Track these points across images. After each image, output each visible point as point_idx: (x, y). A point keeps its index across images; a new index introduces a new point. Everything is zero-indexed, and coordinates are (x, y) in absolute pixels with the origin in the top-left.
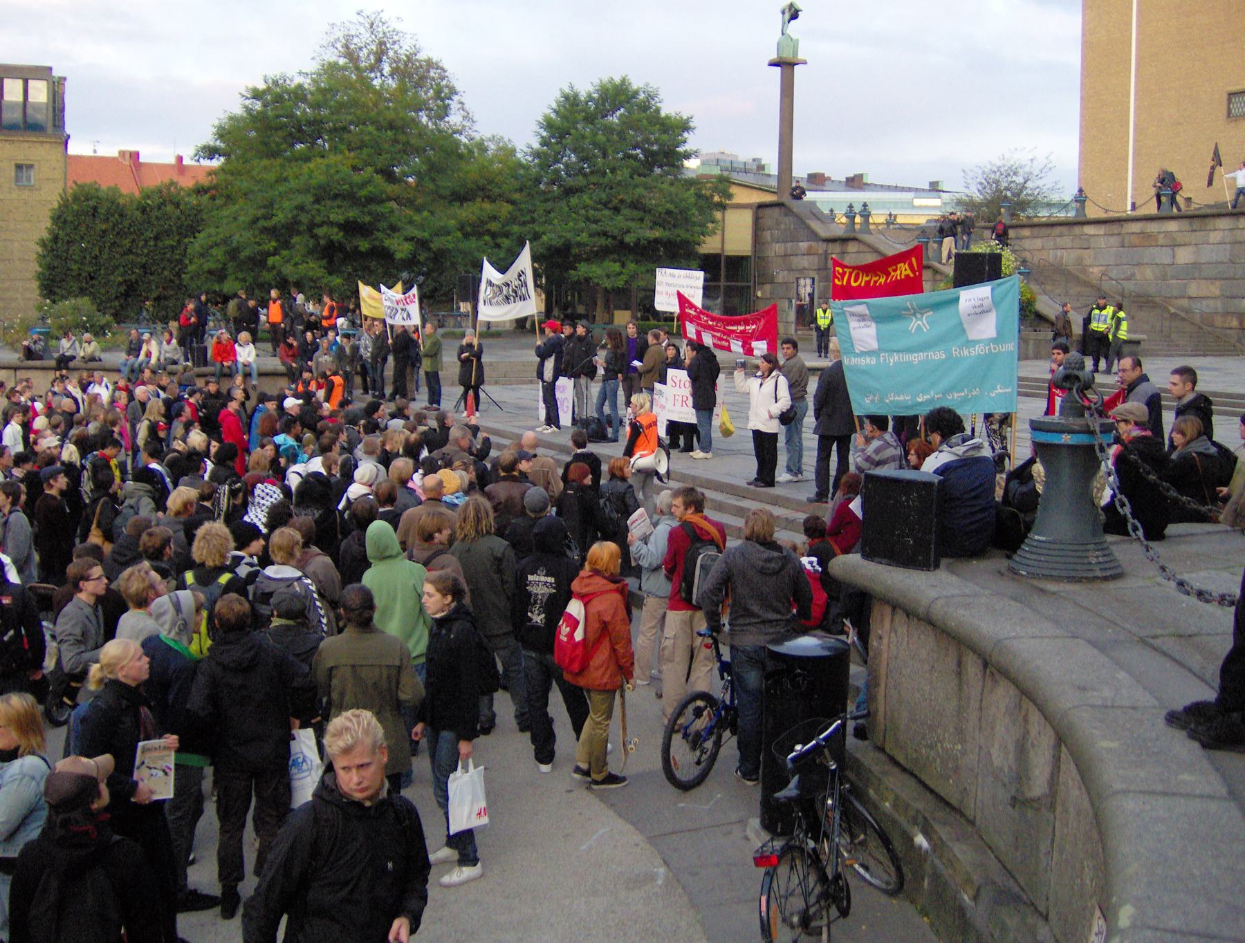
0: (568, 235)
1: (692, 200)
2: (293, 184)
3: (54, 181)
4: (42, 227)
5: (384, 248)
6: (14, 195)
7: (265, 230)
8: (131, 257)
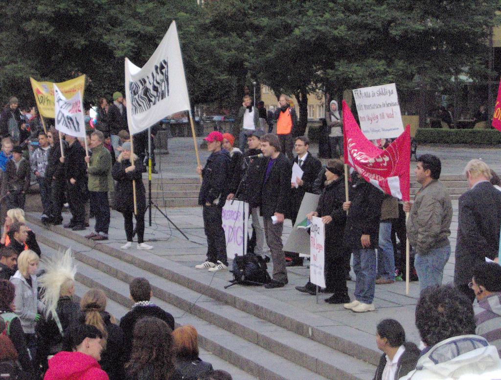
0: (323, 28)
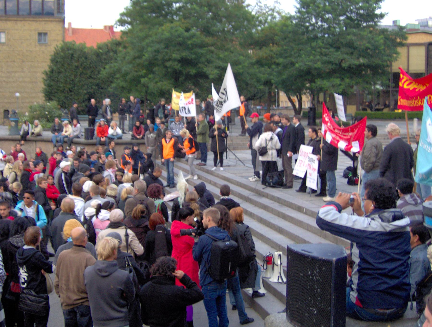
0: (310, 64)
1: (382, 41)
2: (154, 38)
3: (58, 41)
4: (45, 65)
5: (205, 73)
6: (37, 49)
7: (138, 65)
8: (91, 80)
